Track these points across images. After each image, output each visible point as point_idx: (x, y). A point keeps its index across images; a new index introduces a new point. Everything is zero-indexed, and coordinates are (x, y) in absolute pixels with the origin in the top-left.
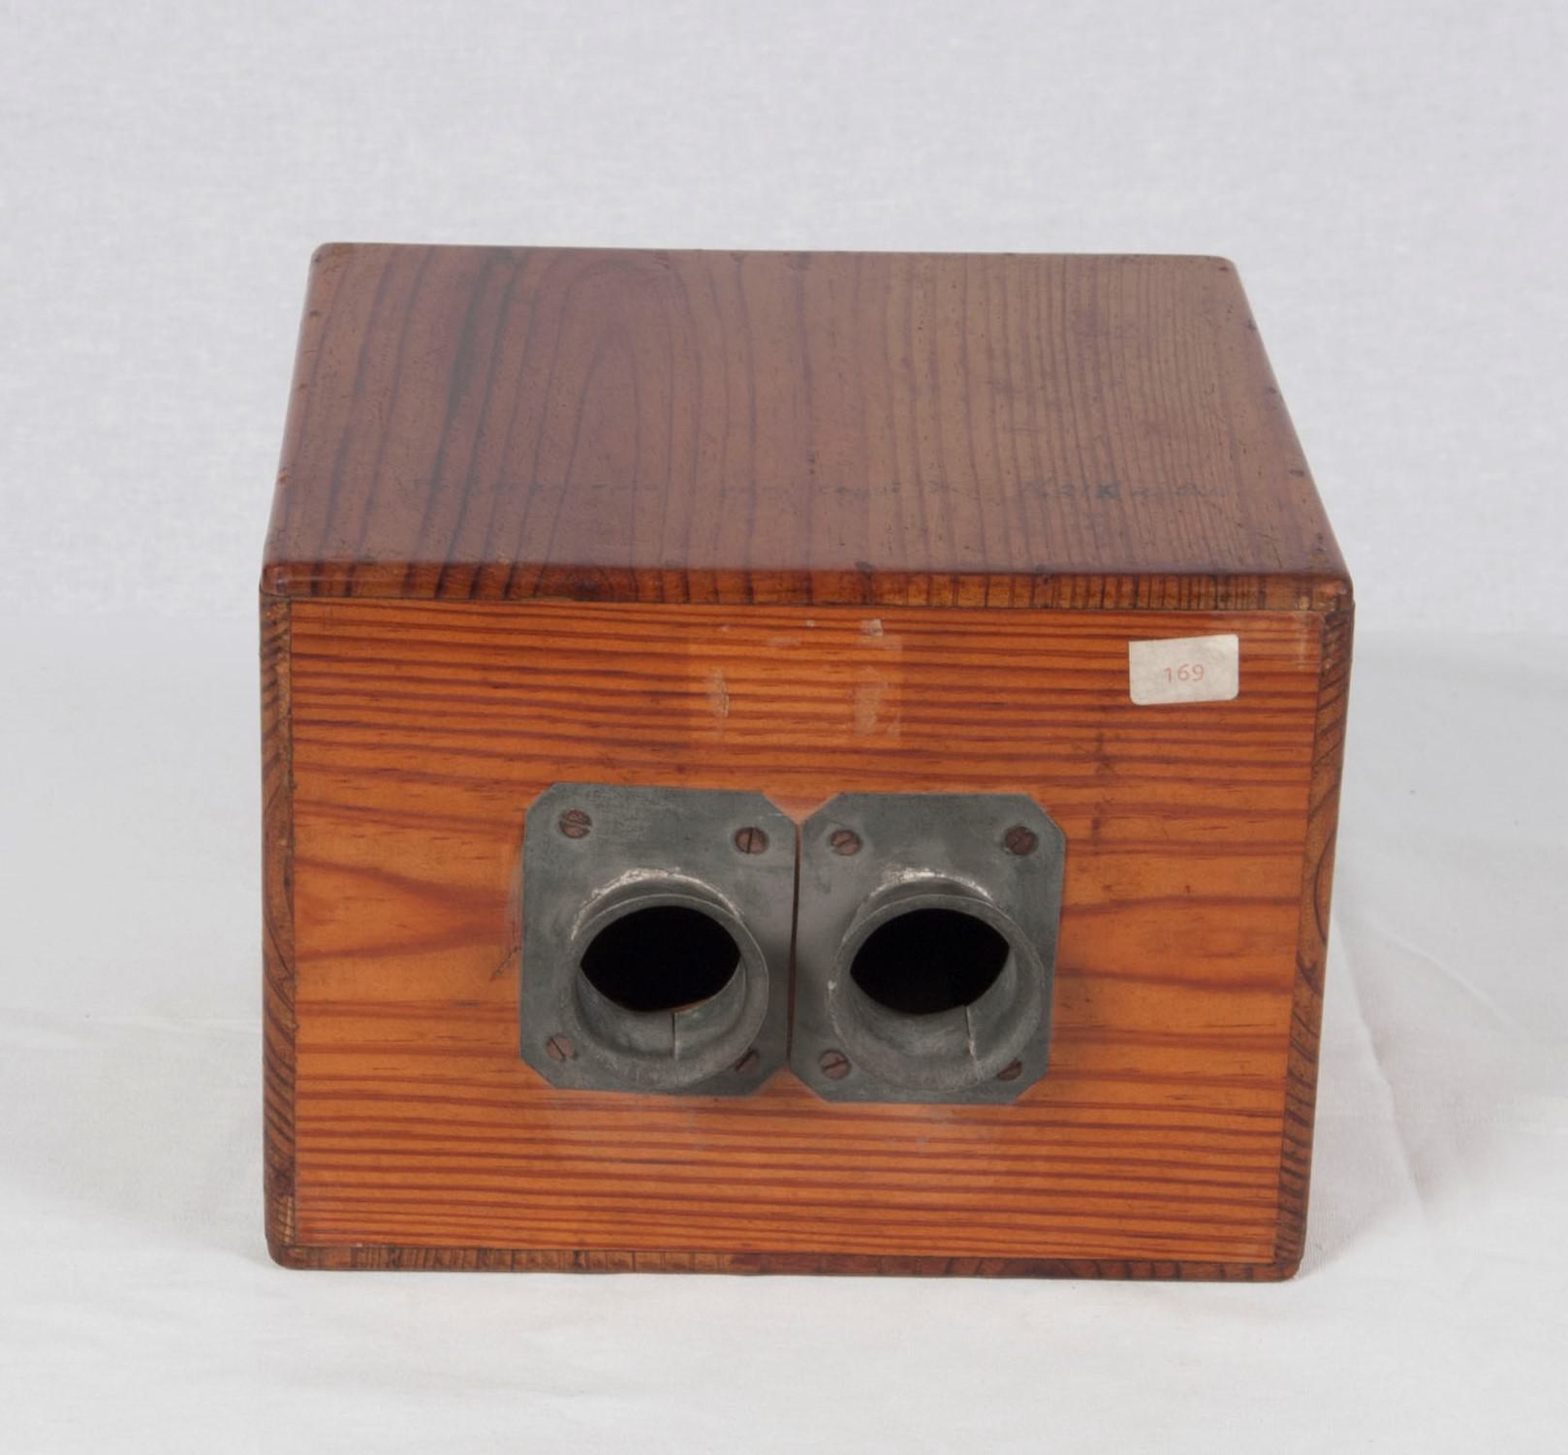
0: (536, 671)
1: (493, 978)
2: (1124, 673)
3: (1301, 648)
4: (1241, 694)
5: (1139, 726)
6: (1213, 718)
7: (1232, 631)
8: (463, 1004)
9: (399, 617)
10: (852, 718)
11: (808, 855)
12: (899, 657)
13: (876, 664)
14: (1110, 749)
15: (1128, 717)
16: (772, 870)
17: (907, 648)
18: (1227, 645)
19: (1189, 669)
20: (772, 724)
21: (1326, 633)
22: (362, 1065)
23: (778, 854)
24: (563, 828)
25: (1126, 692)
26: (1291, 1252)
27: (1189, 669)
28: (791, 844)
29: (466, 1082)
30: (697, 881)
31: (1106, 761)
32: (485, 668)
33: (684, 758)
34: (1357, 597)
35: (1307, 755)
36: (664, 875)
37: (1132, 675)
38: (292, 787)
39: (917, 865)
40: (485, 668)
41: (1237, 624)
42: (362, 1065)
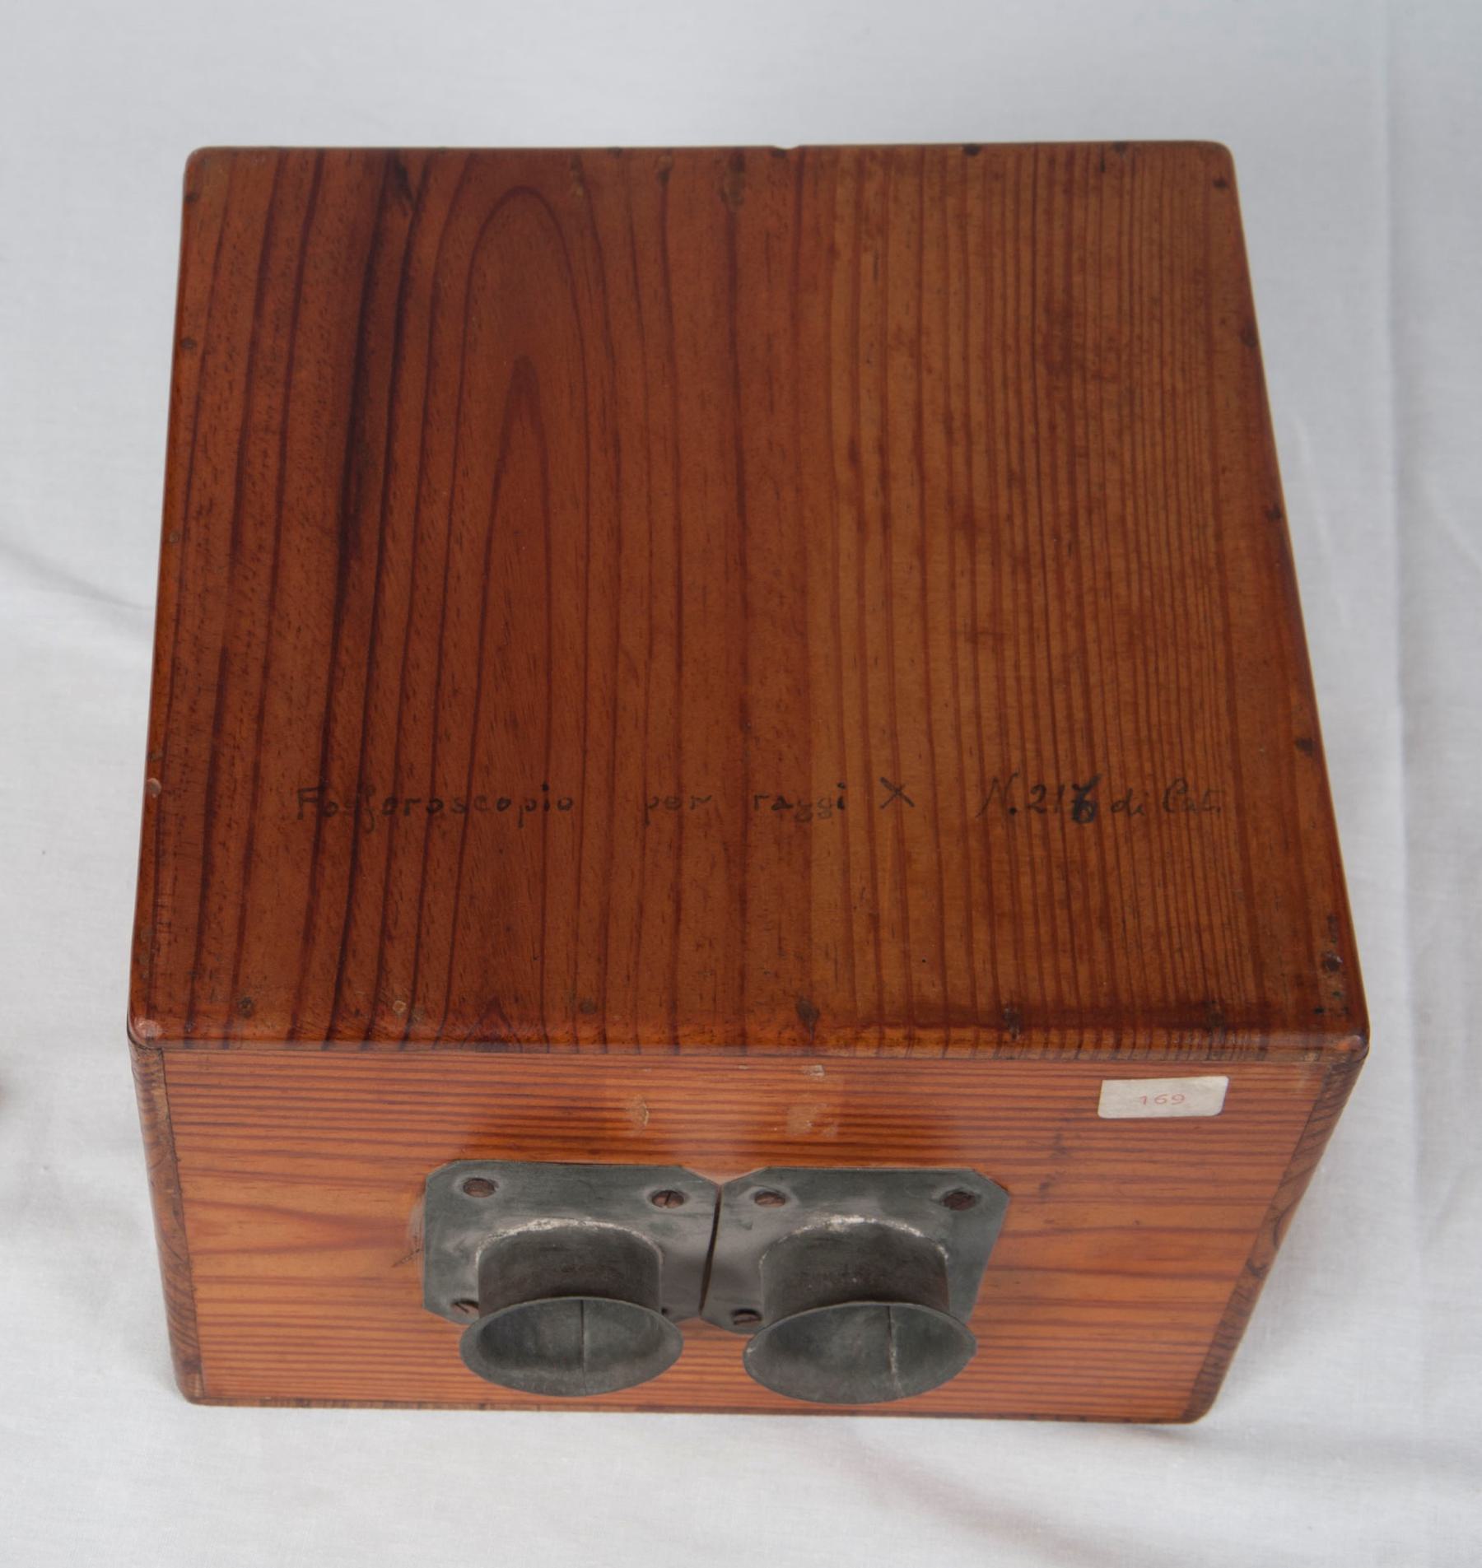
0: (438, 1094)
1: (395, 1265)
2: (1096, 1099)
3: (1301, 1085)
4: (1223, 1112)
5: (1104, 1130)
6: (1192, 1126)
7: (1222, 1074)
8: (371, 1279)
9: (282, 1062)
10: (784, 1124)
11: (728, 1205)
12: (840, 1088)
13: (812, 1092)
14: (1067, 1143)
15: (1093, 1125)
16: (692, 1216)
17: (847, 1082)
18: (1217, 1084)
19: (1169, 1098)
20: (695, 1127)
21: (1331, 1075)
22: (266, 1309)
23: (698, 1204)
24: (501, 809)
25: (1096, 1110)
26: (1052, 162)
27: (1169, 1098)
28: (712, 1199)
29: (370, 1319)
30: (610, 1226)
31: (1063, 1150)
32: (379, 1092)
33: (596, 1145)
34: (1367, 1060)
35: (1291, 1148)
36: (575, 1223)
37: (1102, 1100)
38: (177, 1160)
39: (847, 1213)
40: (379, 1092)
41: (1228, 1070)
42: (266, 1309)
